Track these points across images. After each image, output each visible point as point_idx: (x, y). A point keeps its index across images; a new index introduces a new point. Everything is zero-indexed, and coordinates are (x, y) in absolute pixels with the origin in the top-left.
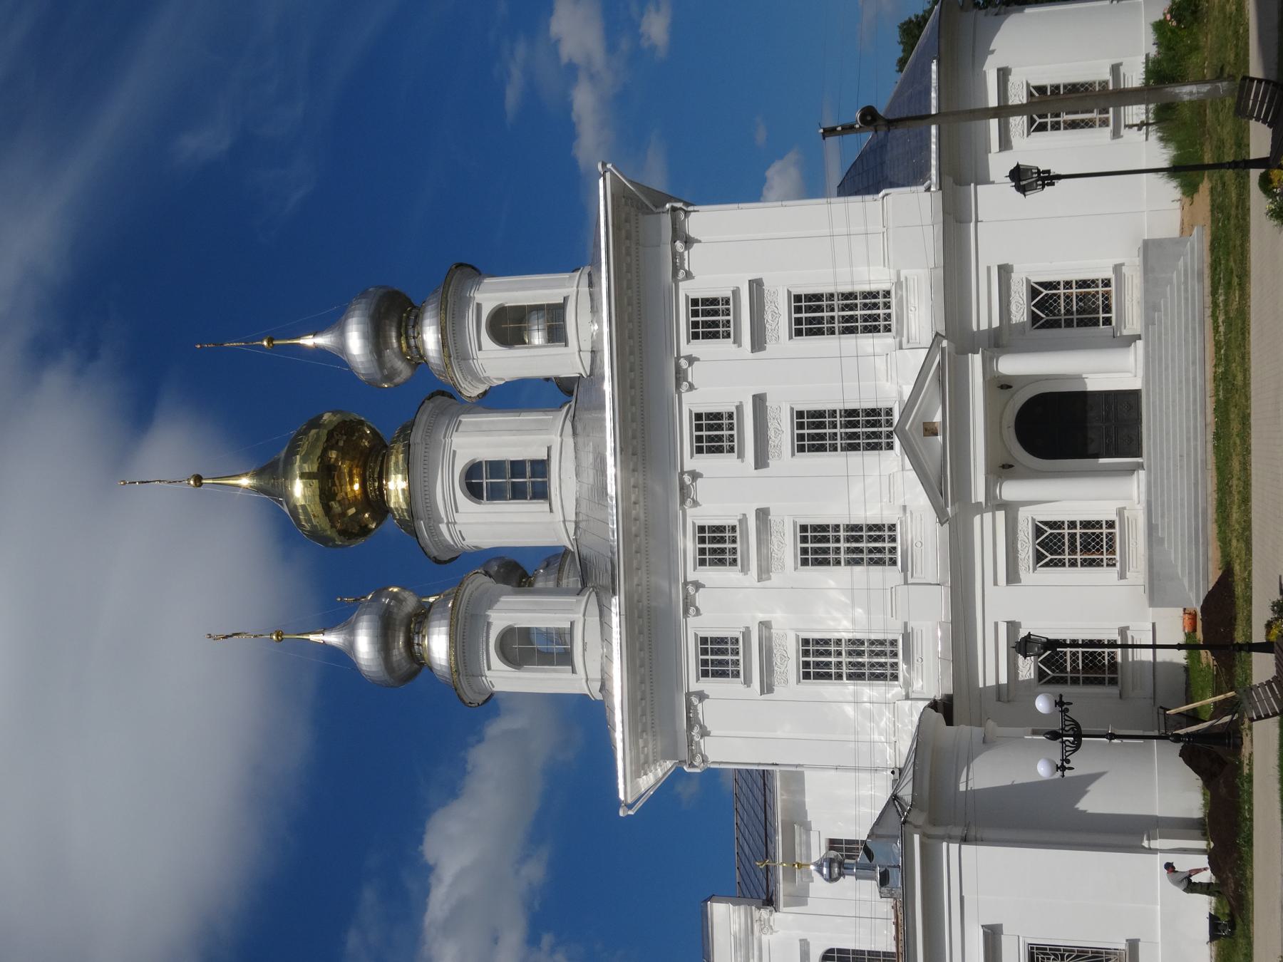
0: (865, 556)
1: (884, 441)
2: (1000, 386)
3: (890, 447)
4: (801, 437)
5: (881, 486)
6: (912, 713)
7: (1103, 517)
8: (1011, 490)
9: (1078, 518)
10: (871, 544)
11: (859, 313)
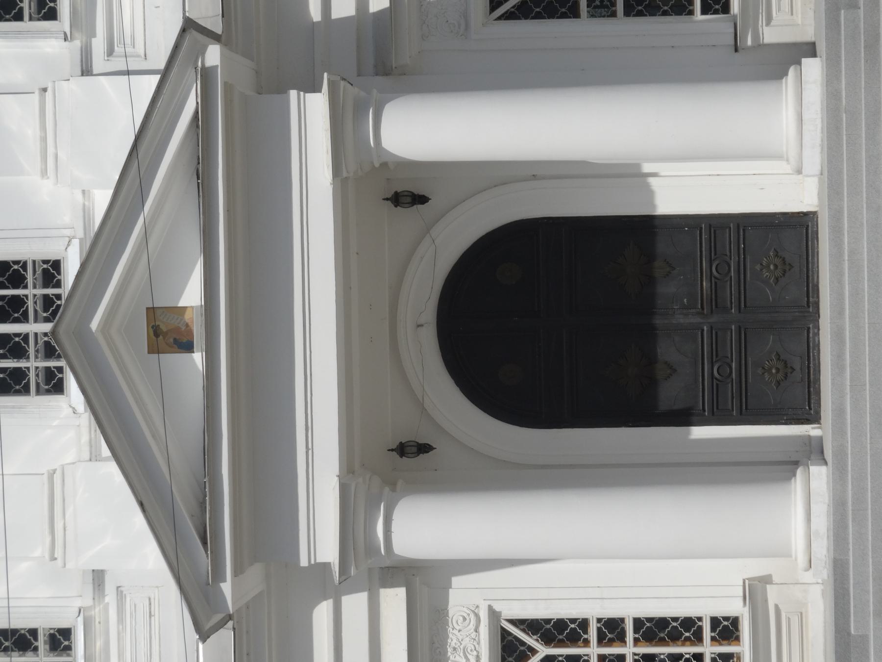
3: (54, 384)
7: (704, 608)
8: (420, 527)
9: (629, 608)
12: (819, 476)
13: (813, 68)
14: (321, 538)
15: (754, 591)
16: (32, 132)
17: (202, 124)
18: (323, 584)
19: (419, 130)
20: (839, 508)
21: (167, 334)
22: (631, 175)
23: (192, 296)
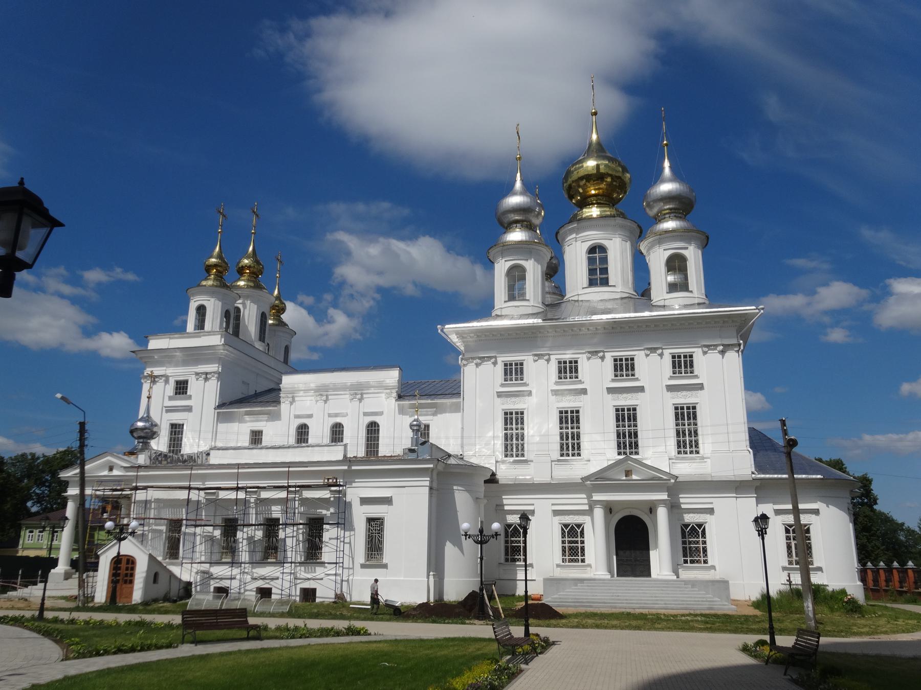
0: (565, 441)
1: (622, 451)
2: (651, 508)
3: (619, 454)
4: (682, 408)
5: (599, 449)
6: (490, 464)
7: (586, 557)
8: (599, 513)
9: (586, 545)
10: (571, 444)
11: (687, 438)
12: (609, 577)
13: (675, 578)
14: (597, 497)
15: (589, 566)
16: (659, 450)
17: (660, 479)
18: (589, 497)
19: (662, 513)
20: (604, 580)
21: (628, 473)
22: (656, 547)
23: (634, 477)
